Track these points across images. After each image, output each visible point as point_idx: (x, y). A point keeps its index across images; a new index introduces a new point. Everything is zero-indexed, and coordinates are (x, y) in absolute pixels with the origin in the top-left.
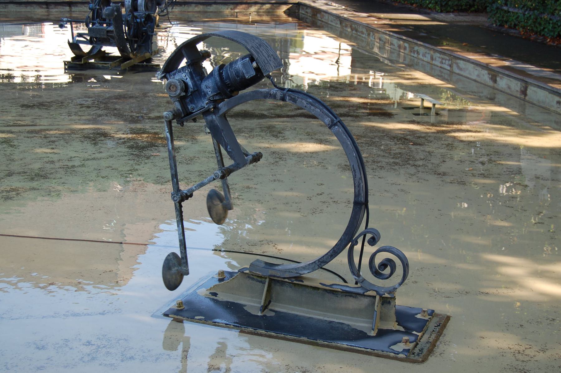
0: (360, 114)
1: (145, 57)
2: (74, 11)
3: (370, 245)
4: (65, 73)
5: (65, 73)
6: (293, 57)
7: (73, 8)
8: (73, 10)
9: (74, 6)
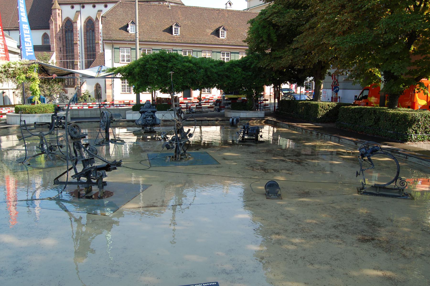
1: (79, 115)
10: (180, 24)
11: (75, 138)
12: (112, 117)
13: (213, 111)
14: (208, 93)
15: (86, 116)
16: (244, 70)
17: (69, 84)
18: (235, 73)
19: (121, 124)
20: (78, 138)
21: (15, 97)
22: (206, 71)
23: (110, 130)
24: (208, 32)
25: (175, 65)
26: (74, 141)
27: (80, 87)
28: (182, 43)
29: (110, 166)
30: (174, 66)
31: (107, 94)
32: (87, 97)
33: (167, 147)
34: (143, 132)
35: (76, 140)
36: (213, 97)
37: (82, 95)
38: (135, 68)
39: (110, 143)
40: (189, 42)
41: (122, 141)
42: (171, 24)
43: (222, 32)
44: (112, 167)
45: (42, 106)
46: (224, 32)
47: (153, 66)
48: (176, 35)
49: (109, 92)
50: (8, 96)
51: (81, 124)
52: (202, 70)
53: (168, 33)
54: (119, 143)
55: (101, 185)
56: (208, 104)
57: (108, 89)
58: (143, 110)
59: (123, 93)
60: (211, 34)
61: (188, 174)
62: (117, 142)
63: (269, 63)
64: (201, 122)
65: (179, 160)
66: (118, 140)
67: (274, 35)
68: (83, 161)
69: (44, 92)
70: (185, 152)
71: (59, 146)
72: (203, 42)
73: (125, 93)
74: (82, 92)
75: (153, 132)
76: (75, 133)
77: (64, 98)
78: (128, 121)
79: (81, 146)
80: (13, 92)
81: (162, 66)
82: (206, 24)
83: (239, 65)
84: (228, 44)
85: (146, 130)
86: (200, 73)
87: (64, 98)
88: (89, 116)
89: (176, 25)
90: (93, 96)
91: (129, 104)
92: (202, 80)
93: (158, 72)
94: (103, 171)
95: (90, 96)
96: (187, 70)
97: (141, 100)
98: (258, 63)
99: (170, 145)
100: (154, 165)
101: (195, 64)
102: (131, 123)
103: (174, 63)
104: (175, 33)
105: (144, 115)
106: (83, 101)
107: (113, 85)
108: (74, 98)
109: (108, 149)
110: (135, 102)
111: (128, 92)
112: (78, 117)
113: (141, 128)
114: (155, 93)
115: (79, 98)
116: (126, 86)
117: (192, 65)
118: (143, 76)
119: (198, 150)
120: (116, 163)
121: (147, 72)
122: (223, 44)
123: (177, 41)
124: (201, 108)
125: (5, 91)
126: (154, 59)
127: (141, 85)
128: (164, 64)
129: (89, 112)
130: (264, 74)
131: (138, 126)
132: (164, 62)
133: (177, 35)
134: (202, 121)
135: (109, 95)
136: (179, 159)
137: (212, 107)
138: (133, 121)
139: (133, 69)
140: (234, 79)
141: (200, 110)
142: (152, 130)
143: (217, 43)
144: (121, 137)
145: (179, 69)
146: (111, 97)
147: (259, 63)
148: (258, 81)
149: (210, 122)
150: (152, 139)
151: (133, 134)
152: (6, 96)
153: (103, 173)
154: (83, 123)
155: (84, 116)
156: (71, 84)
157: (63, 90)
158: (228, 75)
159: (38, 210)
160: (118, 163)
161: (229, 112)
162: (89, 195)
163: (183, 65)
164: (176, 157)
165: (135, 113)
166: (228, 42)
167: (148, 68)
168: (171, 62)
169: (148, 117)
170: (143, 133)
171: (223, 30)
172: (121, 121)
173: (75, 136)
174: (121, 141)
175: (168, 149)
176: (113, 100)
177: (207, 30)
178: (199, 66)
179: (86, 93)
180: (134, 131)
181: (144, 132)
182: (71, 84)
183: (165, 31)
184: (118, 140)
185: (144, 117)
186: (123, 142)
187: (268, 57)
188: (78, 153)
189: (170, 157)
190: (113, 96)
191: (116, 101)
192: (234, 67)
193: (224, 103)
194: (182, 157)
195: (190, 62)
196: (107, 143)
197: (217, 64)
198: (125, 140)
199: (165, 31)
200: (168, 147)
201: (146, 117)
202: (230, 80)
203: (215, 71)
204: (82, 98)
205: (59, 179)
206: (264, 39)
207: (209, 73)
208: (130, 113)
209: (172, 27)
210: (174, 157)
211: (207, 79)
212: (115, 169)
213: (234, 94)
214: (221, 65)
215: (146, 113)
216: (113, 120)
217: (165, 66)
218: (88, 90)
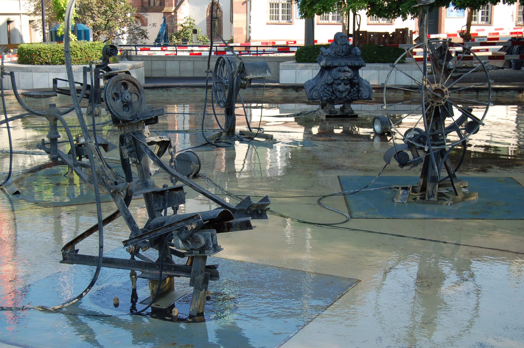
0: (47, 31)
1: (165, 70)
2: (480, 96)
3: (338, 33)
4: (133, 344)
5: (133, 344)
6: (86, 36)
7: (479, 93)
8: (479, 95)
9: (480, 92)
11: (125, 122)
12: (242, 70)
13: (503, 68)
14: (484, 23)
15: (184, 75)
17: (152, 4)
19: (267, 94)
20: (136, 121)
21: (33, 30)
23: (239, 109)
26: (122, 132)
27: (175, 11)
29: (232, 218)
31: (235, 25)
32: (190, 35)
33: (398, 161)
34: (323, 114)
35: (128, 130)
36: (498, 34)
37: (180, 28)
39: (237, 142)
41: (269, 138)
44: (237, 220)
45: (79, 46)
49: (239, 19)
50: (19, 30)
51: (169, 93)
54: (259, 144)
55: (200, 278)
56: (487, 50)
57: (237, 13)
59: (272, 21)
61: (474, 250)
62: (255, 139)
65: (435, 199)
66: (257, 135)
68: (147, 196)
69: (94, 20)
70: (452, 176)
71: (101, 145)
73: (277, 21)
74: (179, 22)
75: (353, 117)
76: (127, 105)
77: (138, 34)
78: (285, 87)
79: (142, 146)
80: (30, 22)
85: (331, 112)
87: (138, 34)
88: (188, 75)
90: (203, 31)
91: (285, 49)
94: (208, 233)
95: (195, 31)
97: (315, 39)
99: (409, 153)
100: (361, 214)
102: (293, 94)
106: (180, 42)
107: (249, 3)
108: (159, 35)
109: (231, 159)
110: (301, 42)
111: (285, 22)
112: (162, 75)
113: (316, 107)
114: (355, 15)
115: (171, 37)
116: (280, 6)
119: (484, 170)
120: (252, 205)
124: (471, 58)
125: (12, 18)
129: (189, 65)
131: (311, 101)
134: (477, 90)
135: (240, 26)
136: (433, 195)
137: (501, 58)
138: (297, 88)
141: (467, 63)
142: (346, 111)
144: (267, 129)
146: (245, 32)
149: (500, 94)
150: (347, 133)
151: (296, 120)
152: (15, 30)
153: (207, 241)
154: (174, 90)
155: (177, 74)
156: (154, 4)
157: (137, 17)
159: (216, 172)
160: (258, 206)
162: (163, 304)
164: (424, 189)
165: (303, 69)
169: (340, 84)
170: (324, 118)
172: (266, 86)
173: (126, 115)
174: (267, 137)
175: (402, 164)
176: (248, 40)
179: (187, 25)
180: (298, 112)
181: (327, 117)
182: (154, 4)
184: (257, 135)
186: (270, 141)
188: (134, 169)
189: (406, 189)
190: (249, 29)
191: (255, 41)
194: (443, 191)
196: (228, 141)
198: (276, 136)
200: (403, 160)
201: (333, 83)
204: (178, 36)
205: (77, 247)
208: (289, 68)
210: (419, 189)
212: (247, 226)
216: (245, 80)
218: (193, 17)
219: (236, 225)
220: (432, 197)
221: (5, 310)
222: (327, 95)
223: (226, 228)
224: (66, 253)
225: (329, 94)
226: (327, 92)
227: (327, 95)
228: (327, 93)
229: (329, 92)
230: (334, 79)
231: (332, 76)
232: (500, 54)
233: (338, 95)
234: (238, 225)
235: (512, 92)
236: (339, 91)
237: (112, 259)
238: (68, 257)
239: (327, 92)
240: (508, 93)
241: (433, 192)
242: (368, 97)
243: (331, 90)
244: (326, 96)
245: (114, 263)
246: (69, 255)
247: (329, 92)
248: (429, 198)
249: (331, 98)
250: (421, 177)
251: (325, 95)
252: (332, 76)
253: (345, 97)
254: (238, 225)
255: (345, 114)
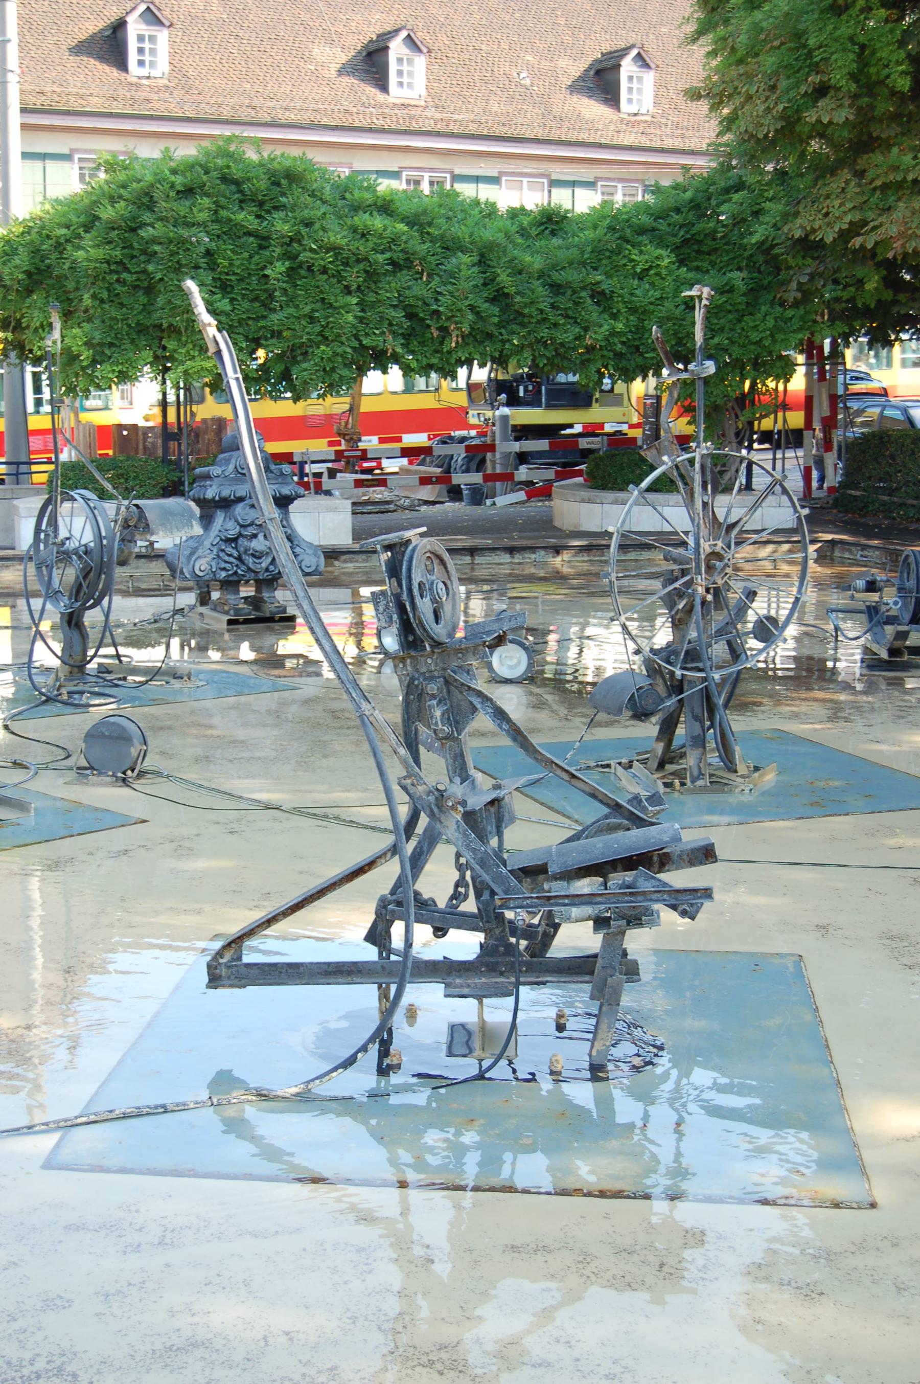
10: (165, 14)
16: (682, 262)
18: (636, 276)
22: (483, 262)
24: (321, 59)
25: (308, 224)
28: (188, 120)
30: (304, 231)
38: (74, 239)
40: (226, 113)
42: (112, 14)
43: (400, 60)
46: (410, 62)
47: (184, 232)
48: (144, 72)
52: (465, 259)
53: (101, 59)
58: (226, 493)
60: (341, 72)
63: (856, 216)
64: (468, 559)
67: (894, 57)
72: (306, 117)
81: (233, 232)
82: (304, 16)
83: (654, 230)
84: (440, 127)
86: (452, 275)
89: (149, 16)
92: (471, 317)
93: (212, 266)
96: (381, 258)
98: (787, 217)
101: (414, 221)
103: (306, 213)
104: (141, 63)
105: (231, 524)
117: (402, 227)
118: (119, 289)
121: (150, 268)
122: (415, 126)
123: (160, 108)
126: (188, 192)
127: (111, 345)
128: (245, 218)
130: (804, 279)
132: (242, 209)
133: (155, 73)
139: (59, 246)
140: (633, 310)
143: (380, 123)
145: (335, 249)
147: (797, 214)
148: (770, 323)
149: (518, 558)
158: (604, 287)
161: (590, 501)
163: (355, 230)
166: (438, 116)
167: (154, 240)
168: (283, 207)
169: (255, 536)
171: (405, 52)
177: (316, 51)
178: (442, 237)
181: (230, 622)
183: (84, 48)
185: (231, 534)
187: (847, 182)
192: (628, 242)
193: (507, 455)
195: (385, 207)
197: (531, 224)
199: (84, 48)
201: (240, 535)
202: (614, 316)
203: (535, 262)
206: (838, 77)
207: (504, 278)
209: (119, 26)
211: (496, 310)
213: (549, 406)
214: (553, 233)
215: (239, 509)
217: (249, 234)
219: (680, 856)
220: (698, 778)
221: (173, 1111)
222: (228, 566)
223: (657, 865)
224: (220, 964)
225: (231, 563)
226: (227, 558)
227: (228, 566)
228: (226, 562)
229: (232, 560)
230: (242, 526)
231: (237, 521)
232: (425, 472)
233: (251, 566)
234: (685, 857)
235: (542, 553)
236: (253, 555)
237: (355, 964)
238: (224, 972)
239: (227, 558)
240: (533, 556)
241: (700, 768)
242: (313, 568)
243: (235, 554)
244: (224, 569)
245: (360, 972)
246: (229, 967)
247: (232, 560)
248: (693, 782)
249: (236, 573)
250: (658, 739)
251: (223, 565)
252: (237, 521)
253: (267, 570)
254: (685, 857)
255: (268, 615)
